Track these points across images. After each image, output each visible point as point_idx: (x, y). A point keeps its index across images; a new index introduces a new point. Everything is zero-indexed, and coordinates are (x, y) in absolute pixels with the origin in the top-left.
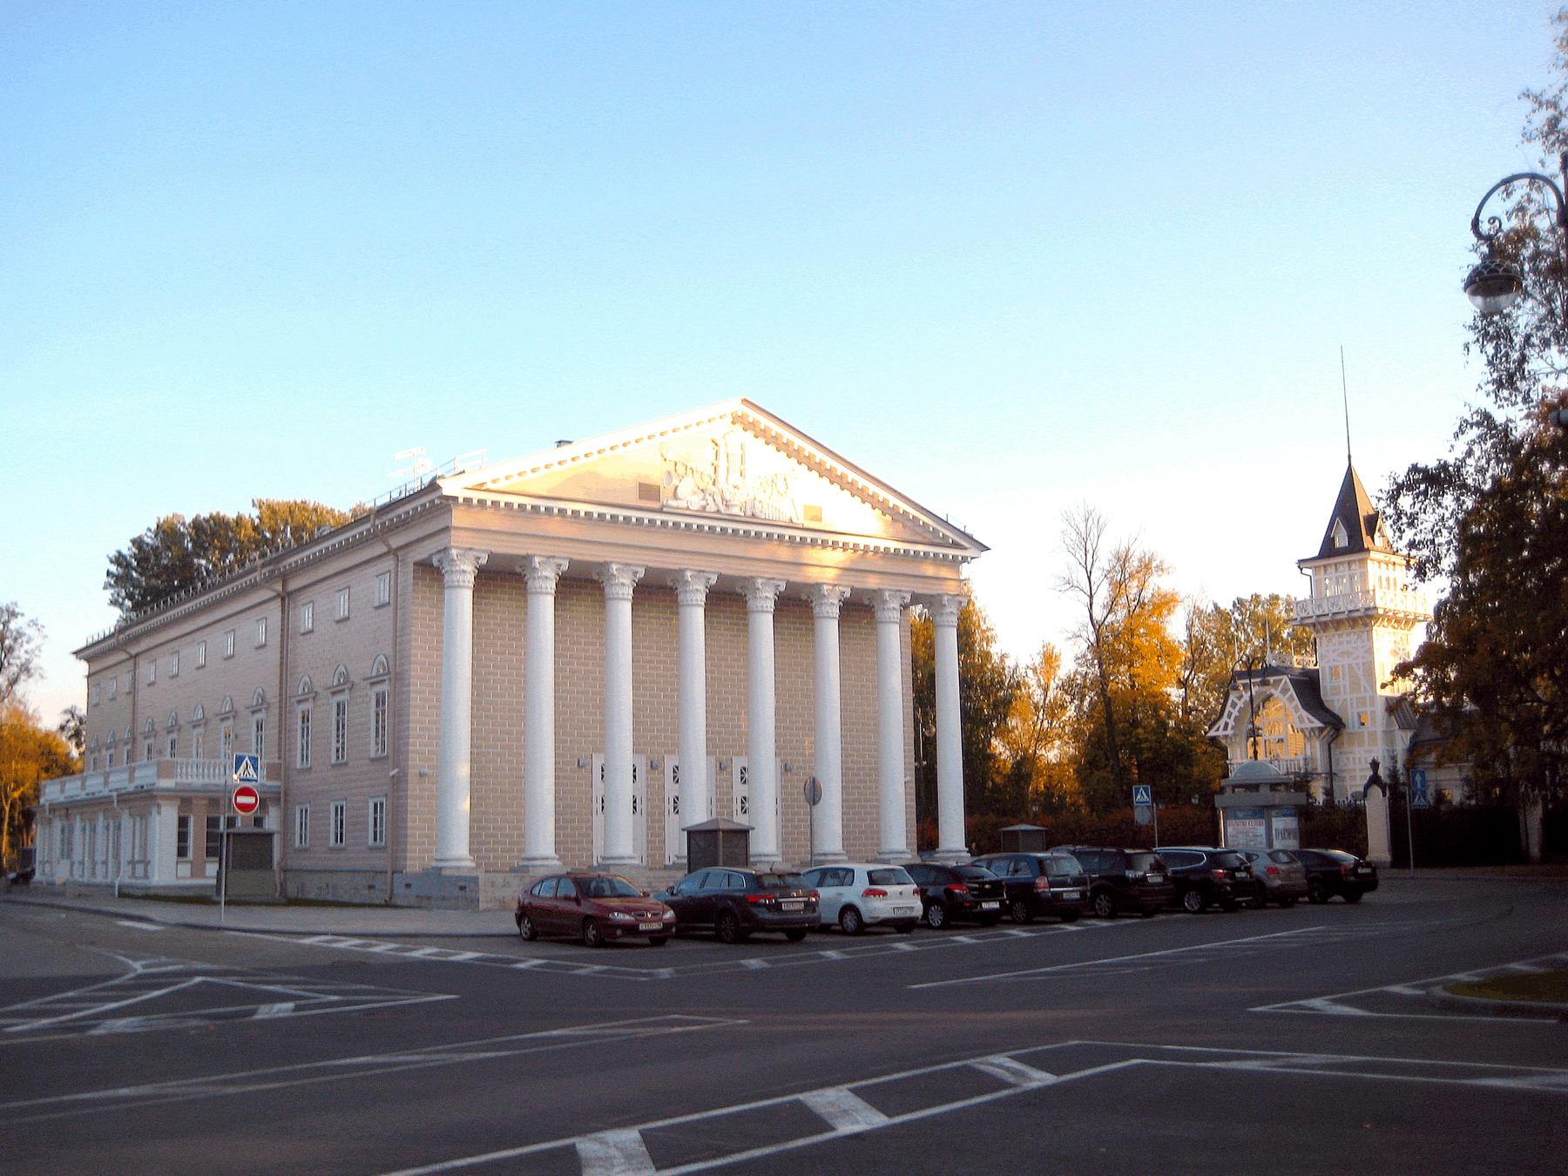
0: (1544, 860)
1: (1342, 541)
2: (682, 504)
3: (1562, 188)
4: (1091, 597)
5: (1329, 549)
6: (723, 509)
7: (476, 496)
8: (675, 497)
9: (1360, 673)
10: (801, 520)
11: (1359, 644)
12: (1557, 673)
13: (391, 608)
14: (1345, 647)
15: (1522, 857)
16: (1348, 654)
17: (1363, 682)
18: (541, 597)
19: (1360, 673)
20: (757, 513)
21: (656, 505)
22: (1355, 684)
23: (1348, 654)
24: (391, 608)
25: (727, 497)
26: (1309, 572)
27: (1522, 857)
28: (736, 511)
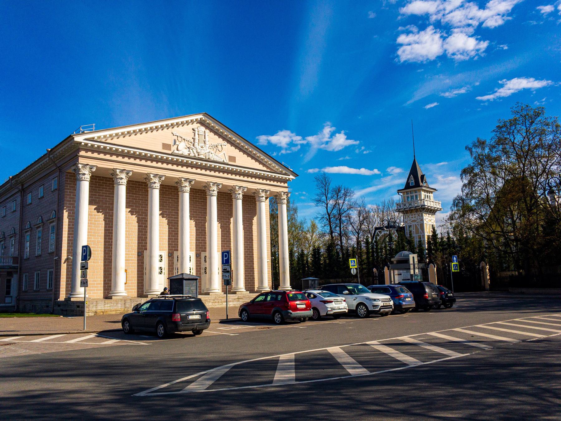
0: (491, 289)
1: (412, 182)
2: (180, 153)
3: (257, 300)
4: (327, 204)
5: (408, 186)
6: (197, 155)
7: (90, 143)
8: (177, 150)
9: (419, 227)
10: (227, 161)
11: (419, 218)
12: (541, 206)
13: (57, 192)
14: (414, 219)
15: (483, 289)
16: (415, 221)
17: (420, 230)
18: (120, 186)
19: (419, 227)
20: (210, 158)
21: (170, 152)
22: (417, 232)
23: (415, 221)
24: (57, 192)
25: (199, 151)
26: (402, 194)
27: (483, 289)
28: (202, 156)
